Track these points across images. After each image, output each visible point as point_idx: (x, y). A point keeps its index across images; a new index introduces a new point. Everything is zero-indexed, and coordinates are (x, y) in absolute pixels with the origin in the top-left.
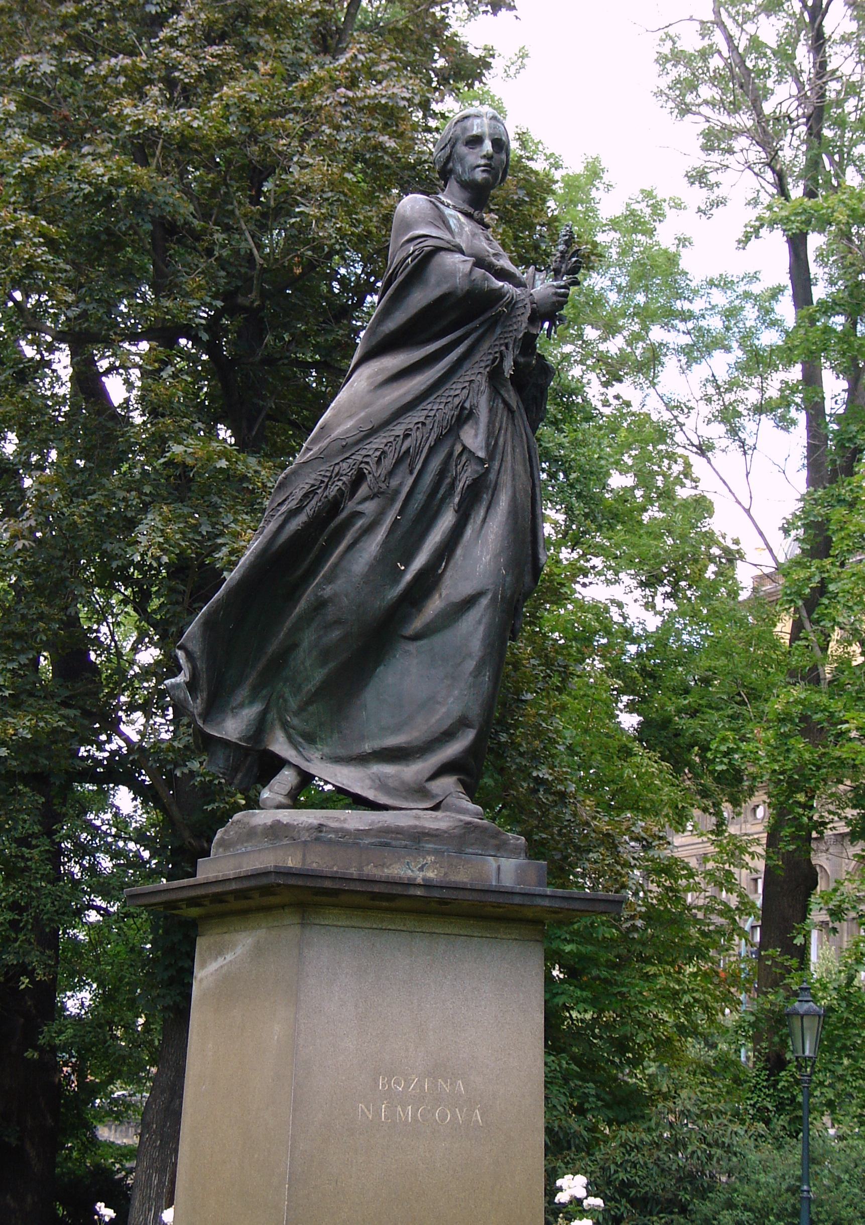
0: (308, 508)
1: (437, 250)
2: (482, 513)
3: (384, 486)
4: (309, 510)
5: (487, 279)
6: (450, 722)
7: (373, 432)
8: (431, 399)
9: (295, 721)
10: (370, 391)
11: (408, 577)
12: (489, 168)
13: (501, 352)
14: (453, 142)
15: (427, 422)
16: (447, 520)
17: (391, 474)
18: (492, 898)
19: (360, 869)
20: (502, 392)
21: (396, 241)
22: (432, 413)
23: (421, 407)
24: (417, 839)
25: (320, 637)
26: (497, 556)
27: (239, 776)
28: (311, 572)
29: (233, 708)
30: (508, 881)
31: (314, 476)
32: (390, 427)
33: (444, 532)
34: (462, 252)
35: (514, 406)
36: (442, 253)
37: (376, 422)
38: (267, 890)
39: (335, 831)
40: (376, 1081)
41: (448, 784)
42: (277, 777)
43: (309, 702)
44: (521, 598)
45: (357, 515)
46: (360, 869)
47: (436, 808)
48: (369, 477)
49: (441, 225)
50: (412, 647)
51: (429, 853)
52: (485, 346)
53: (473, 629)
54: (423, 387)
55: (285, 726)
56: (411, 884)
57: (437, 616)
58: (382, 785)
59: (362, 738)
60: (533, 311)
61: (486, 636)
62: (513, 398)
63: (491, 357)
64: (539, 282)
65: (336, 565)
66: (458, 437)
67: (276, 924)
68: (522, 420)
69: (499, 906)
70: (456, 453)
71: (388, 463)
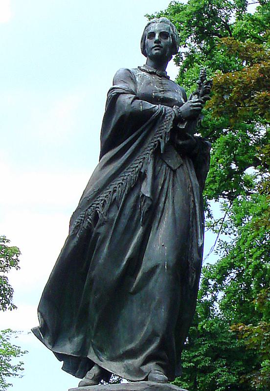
1: (118, 94)
10: (100, 171)
13: (158, 141)
15: (124, 183)
17: (109, 211)
27: (78, 371)
33: (138, 237)
37: (100, 187)
63: (153, 144)
64: (193, 98)
71: (107, 206)
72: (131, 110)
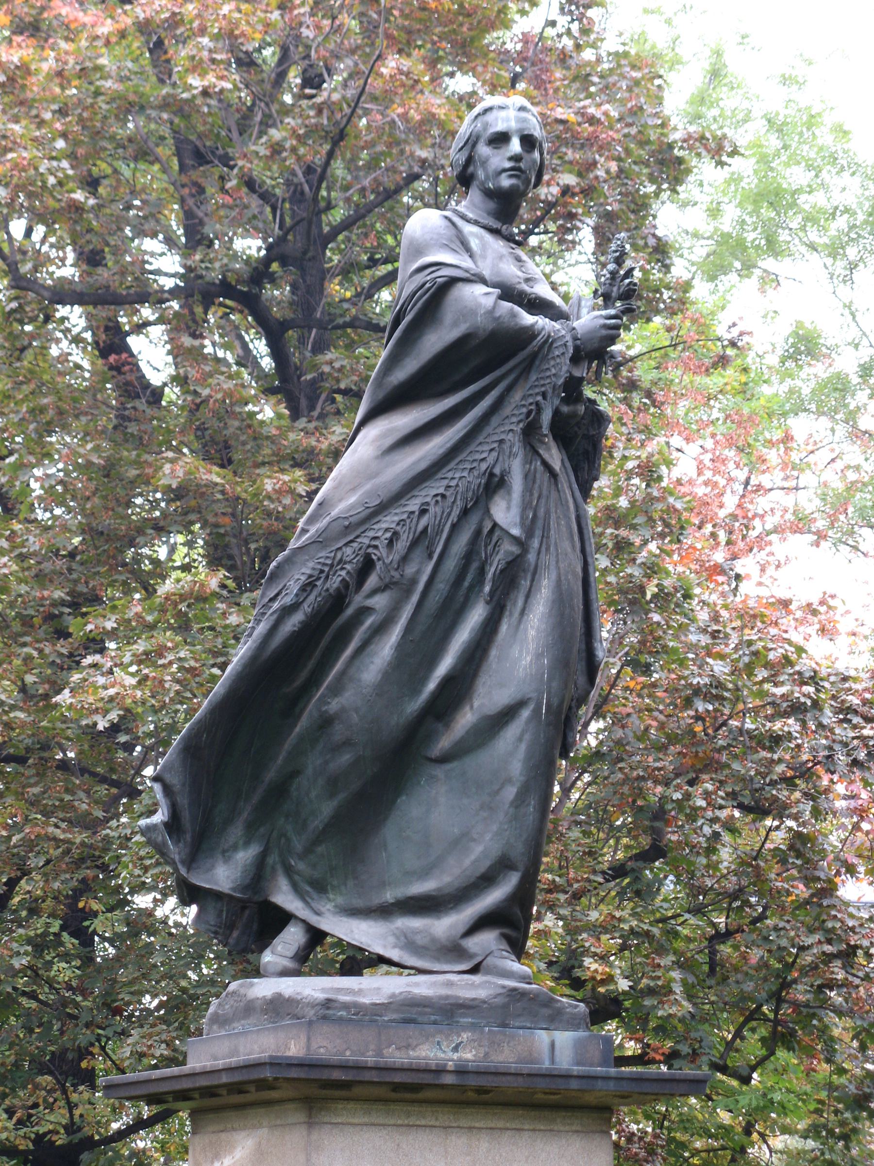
0: (305, 605)
1: (453, 281)
2: (520, 603)
3: (396, 575)
4: (307, 608)
5: (514, 315)
6: (487, 863)
7: (382, 508)
8: (452, 465)
9: (301, 866)
10: (377, 458)
11: (432, 685)
12: (516, 171)
13: (537, 404)
14: (472, 142)
15: (448, 494)
16: (476, 615)
17: (405, 559)
18: (542, 1084)
19: (379, 1054)
20: (541, 452)
21: (405, 270)
22: (453, 483)
23: (440, 475)
24: (448, 1013)
25: (326, 763)
26: (539, 656)
27: (235, 934)
28: (315, 680)
29: (224, 852)
30: (565, 1061)
31: (311, 564)
32: (403, 502)
33: (473, 629)
34: (483, 281)
35: (557, 466)
36: (460, 285)
37: (385, 495)
38: (262, 1085)
39: (346, 1006)
41: (487, 941)
42: (281, 935)
43: (317, 841)
44: (574, 704)
45: (365, 611)
46: (379, 1054)
47: (475, 970)
48: (379, 565)
49: (457, 245)
50: (439, 771)
51: (465, 1028)
52: (517, 396)
53: (512, 748)
54: (441, 451)
55: (289, 871)
56: (440, 1071)
57: (467, 732)
58: (410, 944)
59: (383, 885)
60: (577, 349)
61: (529, 756)
62: (555, 457)
63: (524, 410)
65: (343, 673)
66: (487, 511)
67: (279, 1122)
68: (567, 482)
70: (486, 531)
71: (401, 546)
72: (490, 326)
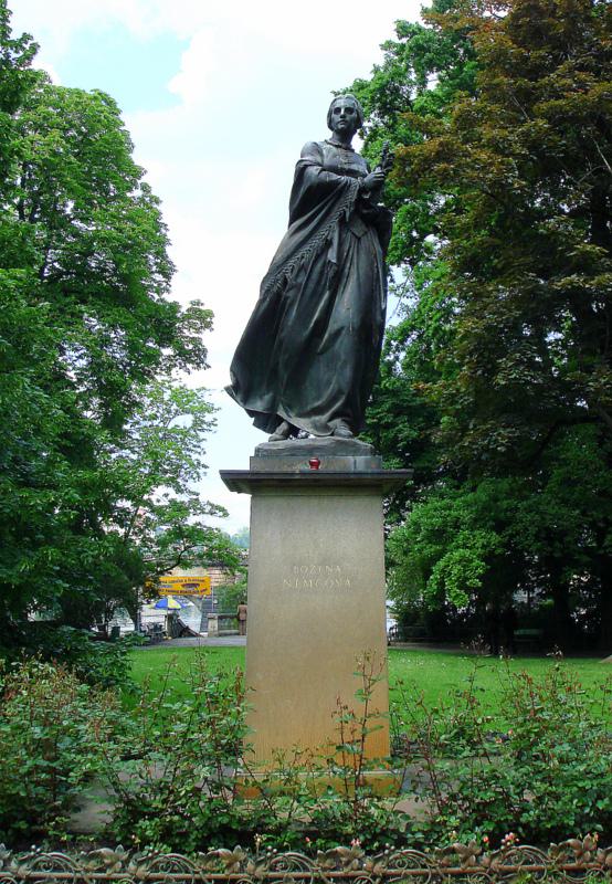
1: (306, 166)
17: (297, 276)
30: (361, 468)
40: (292, 569)
56: (293, 474)
69: (346, 480)
71: (295, 271)
